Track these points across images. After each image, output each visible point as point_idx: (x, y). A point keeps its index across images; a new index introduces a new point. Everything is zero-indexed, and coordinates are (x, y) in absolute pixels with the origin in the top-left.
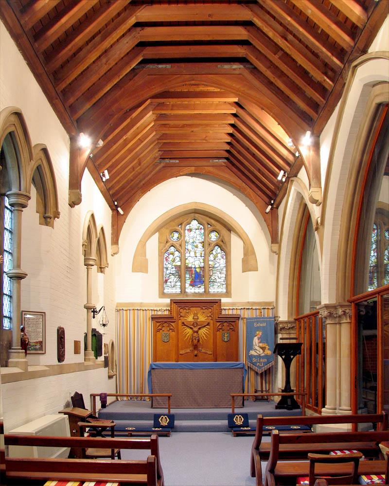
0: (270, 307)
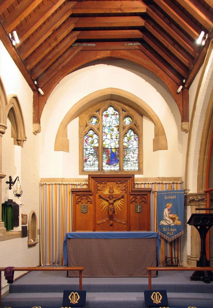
0: (179, 182)
